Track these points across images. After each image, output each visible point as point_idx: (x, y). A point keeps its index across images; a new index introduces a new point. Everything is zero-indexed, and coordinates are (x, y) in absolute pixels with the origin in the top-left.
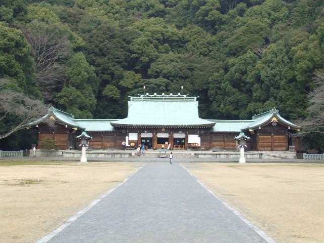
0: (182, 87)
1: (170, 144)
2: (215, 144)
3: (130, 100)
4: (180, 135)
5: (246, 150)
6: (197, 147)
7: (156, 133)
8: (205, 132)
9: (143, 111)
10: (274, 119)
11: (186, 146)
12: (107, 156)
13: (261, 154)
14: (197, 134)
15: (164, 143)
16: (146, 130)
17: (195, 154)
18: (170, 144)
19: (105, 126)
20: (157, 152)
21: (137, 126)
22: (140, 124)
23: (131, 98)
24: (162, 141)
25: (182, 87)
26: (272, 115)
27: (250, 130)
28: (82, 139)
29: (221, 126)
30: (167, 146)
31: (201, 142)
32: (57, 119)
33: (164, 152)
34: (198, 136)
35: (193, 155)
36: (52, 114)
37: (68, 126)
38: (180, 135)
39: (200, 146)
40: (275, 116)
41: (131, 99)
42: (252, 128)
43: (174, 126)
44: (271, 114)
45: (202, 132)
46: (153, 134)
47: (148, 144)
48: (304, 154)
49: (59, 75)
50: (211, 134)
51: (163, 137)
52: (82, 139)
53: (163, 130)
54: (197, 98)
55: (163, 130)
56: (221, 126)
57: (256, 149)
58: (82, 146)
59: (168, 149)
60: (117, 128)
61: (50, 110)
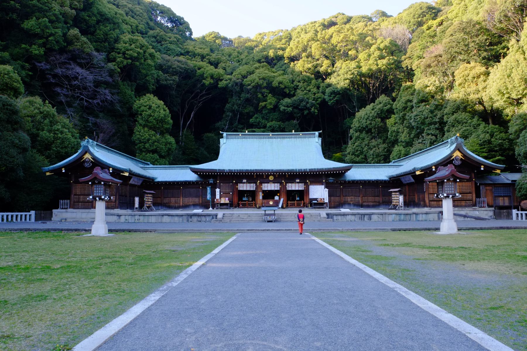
2: (349, 199)
3: (222, 137)
4: (295, 186)
5: (456, 203)
6: (322, 204)
8: (333, 180)
9: (238, 152)
10: (458, 154)
11: (307, 201)
12: (176, 219)
14: (321, 183)
15: (274, 198)
16: (246, 179)
17: (328, 215)
19: (184, 174)
20: (261, 211)
21: (230, 171)
23: (225, 134)
24: (269, 195)
26: (454, 146)
28: (93, 183)
30: (276, 204)
31: (330, 195)
32: (94, 158)
33: (273, 212)
34: (323, 186)
36: (87, 151)
37: (113, 169)
39: (327, 201)
40: (458, 149)
41: (225, 134)
44: (451, 145)
45: (331, 180)
46: (256, 185)
47: (242, 200)
48: (515, 212)
50: (341, 184)
52: (93, 183)
53: (271, 178)
54: (319, 134)
55: (271, 178)
56: (358, 173)
58: (94, 198)
59: (280, 206)
60: (204, 175)
61: (84, 143)
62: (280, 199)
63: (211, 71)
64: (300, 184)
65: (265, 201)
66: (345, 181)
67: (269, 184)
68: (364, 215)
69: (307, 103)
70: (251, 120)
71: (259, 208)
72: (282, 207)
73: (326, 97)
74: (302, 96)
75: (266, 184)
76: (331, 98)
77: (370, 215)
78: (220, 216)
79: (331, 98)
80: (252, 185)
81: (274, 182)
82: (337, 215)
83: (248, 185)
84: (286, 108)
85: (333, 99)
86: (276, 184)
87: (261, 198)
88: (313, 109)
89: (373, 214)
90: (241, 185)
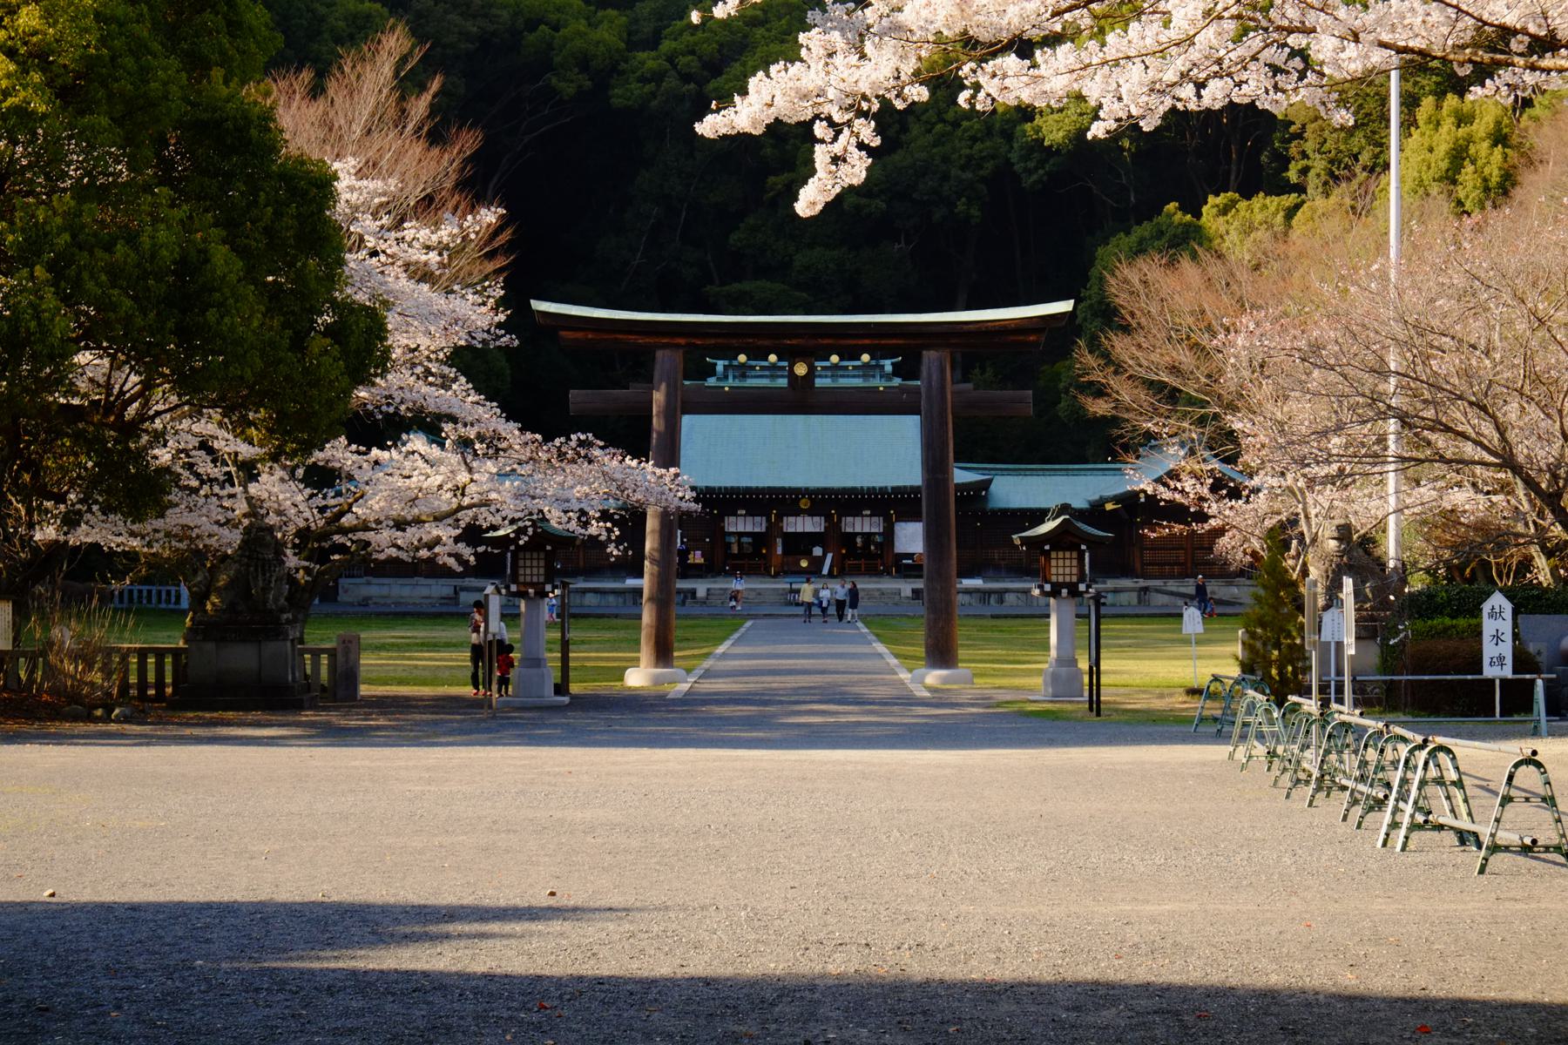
0: (270, 278)
1: (830, 556)
4: (862, 524)
7: (779, 518)
12: (611, 598)
13: (1146, 589)
18: (830, 556)
22: (723, 484)
24: (799, 544)
25: (270, 278)
27: (1109, 507)
29: (1014, 489)
35: (909, 593)
38: (862, 524)
42: (1116, 499)
43: (844, 491)
46: (769, 520)
49: (1150, 1003)
51: (1154, 748)
57: (1126, 571)
59: (825, 571)
62: (825, 555)
63: (578, 43)
64: (875, 519)
65: (790, 559)
66: (984, 512)
67: (800, 519)
68: (990, 592)
69: (946, 177)
70: (734, 237)
71: (776, 575)
72: (831, 575)
73: (1014, 157)
74: (924, 155)
75: (792, 519)
76: (1031, 165)
77: (1001, 593)
78: (701, 593)
79: (1031, 165)
80: (758, 519)
81: (811, 513)
82: (1158, 591)
83: (749, 519)
84: (864, 201)
85: (1036, 169)
86: (817, 519)
87: (779, 551)
88: (961, 206)
89: (1007, 591)
90: (732, 519)
